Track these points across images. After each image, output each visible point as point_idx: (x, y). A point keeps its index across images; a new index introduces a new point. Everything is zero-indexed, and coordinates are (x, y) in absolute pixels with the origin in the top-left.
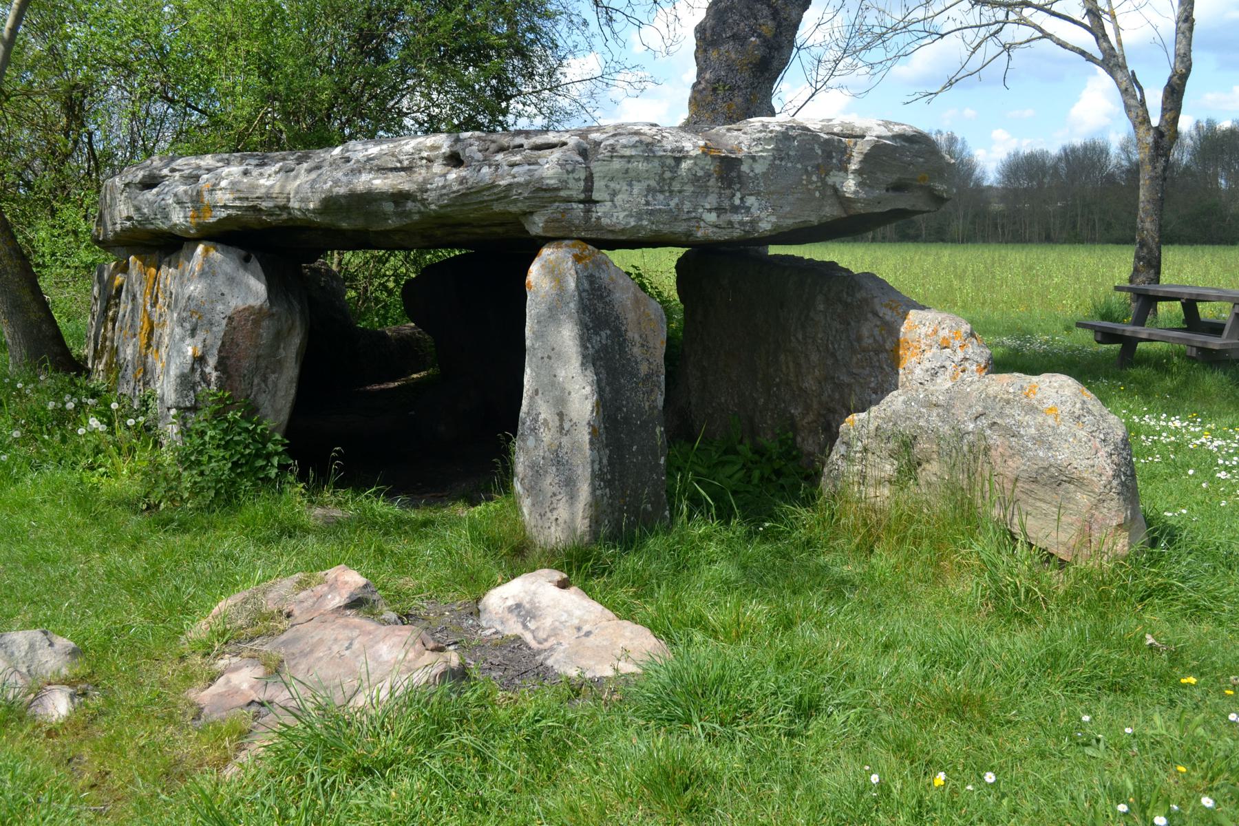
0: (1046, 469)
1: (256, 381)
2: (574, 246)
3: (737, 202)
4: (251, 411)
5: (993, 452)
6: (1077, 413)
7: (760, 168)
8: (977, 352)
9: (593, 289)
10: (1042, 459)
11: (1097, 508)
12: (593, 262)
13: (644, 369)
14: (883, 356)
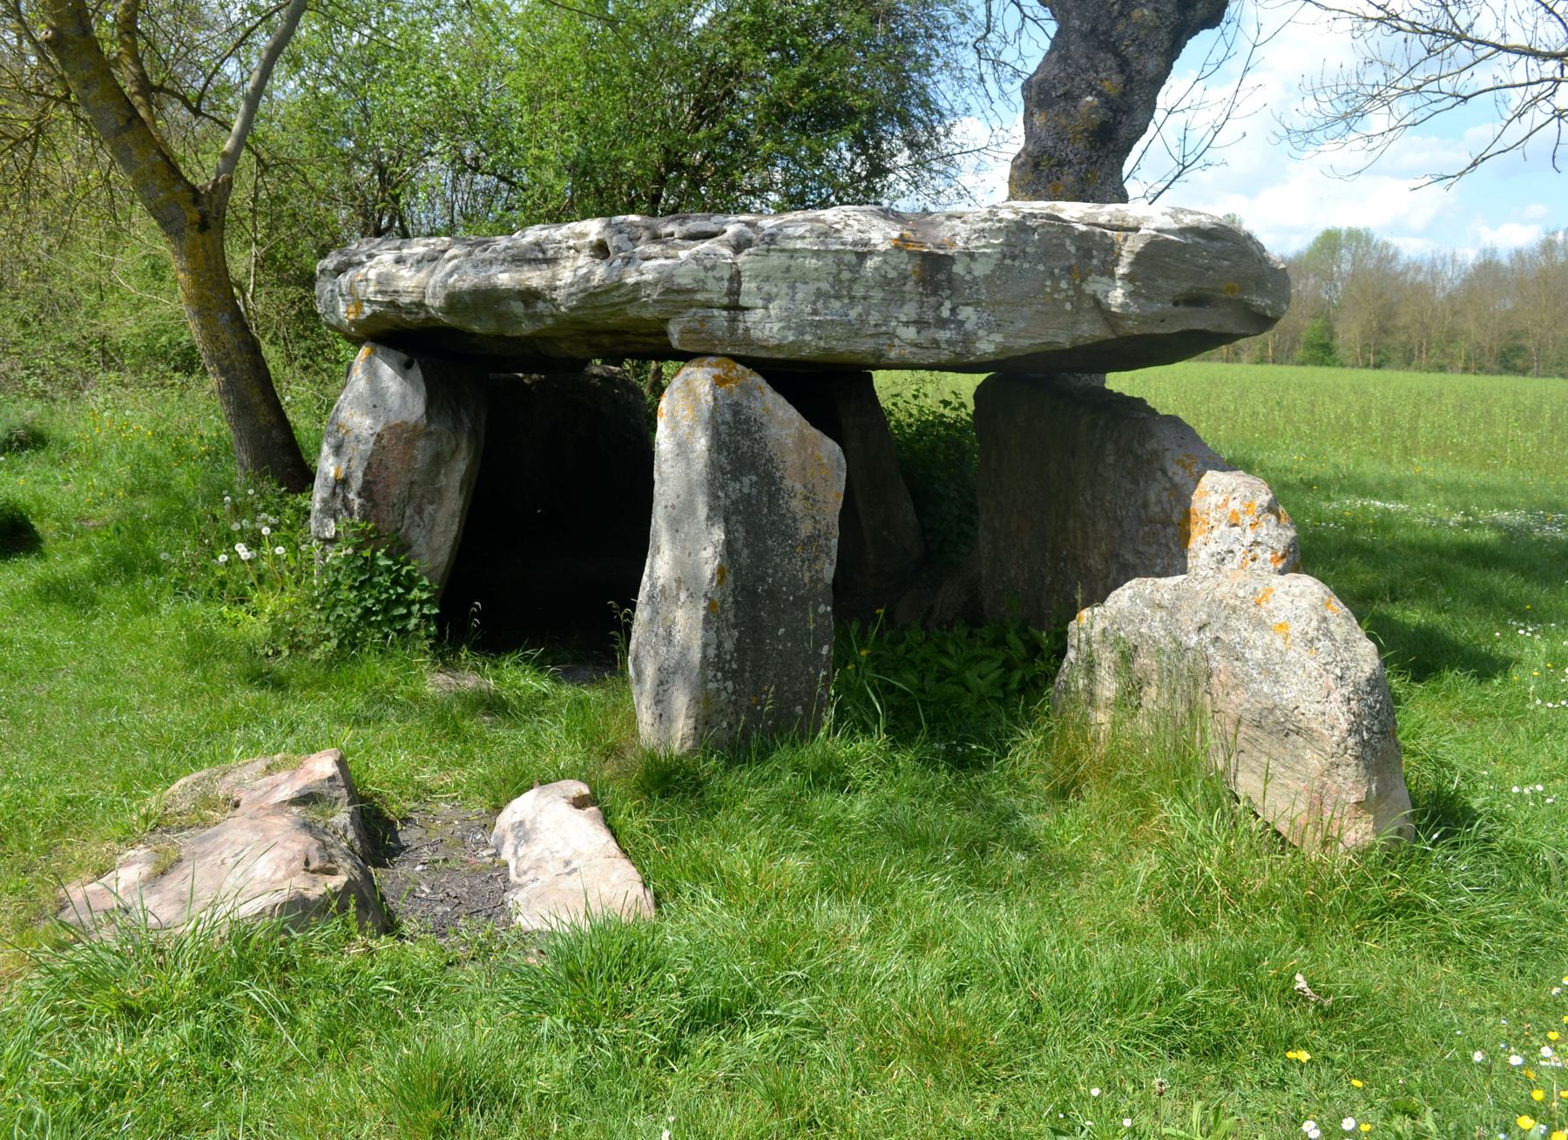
0: (1271, 711)
1: (408, 513)
2: (717, 365)
3: (946, 313)
4: (400, 548)
5: (1214, 680)
6: (1312, 633)
7: (980, 269)
8: (1276, 535)
9: (735, 422)
10: (1266, 696)
11: (1329, 775)
12: (741, 387)
13: (806, 529)
14: (1170, 530)
